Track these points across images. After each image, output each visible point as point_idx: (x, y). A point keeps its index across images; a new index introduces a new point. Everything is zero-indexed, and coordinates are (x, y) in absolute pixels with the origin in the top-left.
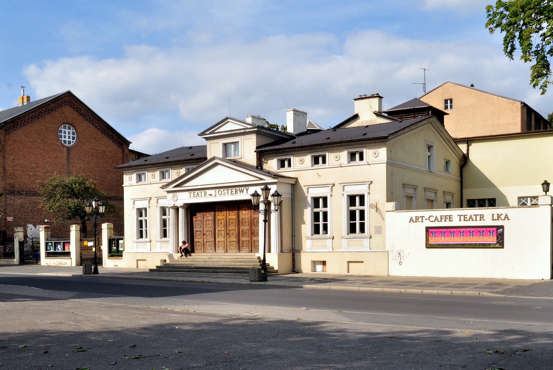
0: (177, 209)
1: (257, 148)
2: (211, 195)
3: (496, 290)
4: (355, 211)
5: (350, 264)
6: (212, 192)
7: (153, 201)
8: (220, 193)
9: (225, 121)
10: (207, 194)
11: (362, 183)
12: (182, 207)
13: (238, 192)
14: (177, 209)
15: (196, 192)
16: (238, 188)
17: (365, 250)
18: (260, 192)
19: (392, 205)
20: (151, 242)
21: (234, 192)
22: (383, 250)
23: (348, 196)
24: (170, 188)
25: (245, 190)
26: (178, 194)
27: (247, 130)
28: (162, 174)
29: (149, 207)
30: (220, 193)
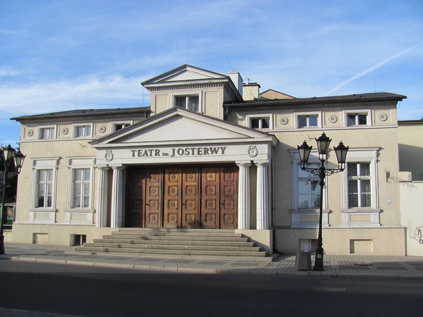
0: (109, 171)
1: (225, 103)
2: (166, 154)
4: (356, 181)
5: (404, 229)
6: (169, 151)
7: (64, 162)
8: (181, 152)
9: (182, 69)
10: (161, 153)
11: (369, 149)
12: (118, 168)
13: (209, 152)
14: (109, 171)
15: (144, 150)
16: (208, 147)
17: (374, 226)
19: (406, 175)
21: (203, 152)
23: (71, 235)
24: (104, 144)
25: (220, 151)
26: (114, 151)
27: (214, 81)
28: (77, 129)
29: (57, 169)
30: (181, 152)
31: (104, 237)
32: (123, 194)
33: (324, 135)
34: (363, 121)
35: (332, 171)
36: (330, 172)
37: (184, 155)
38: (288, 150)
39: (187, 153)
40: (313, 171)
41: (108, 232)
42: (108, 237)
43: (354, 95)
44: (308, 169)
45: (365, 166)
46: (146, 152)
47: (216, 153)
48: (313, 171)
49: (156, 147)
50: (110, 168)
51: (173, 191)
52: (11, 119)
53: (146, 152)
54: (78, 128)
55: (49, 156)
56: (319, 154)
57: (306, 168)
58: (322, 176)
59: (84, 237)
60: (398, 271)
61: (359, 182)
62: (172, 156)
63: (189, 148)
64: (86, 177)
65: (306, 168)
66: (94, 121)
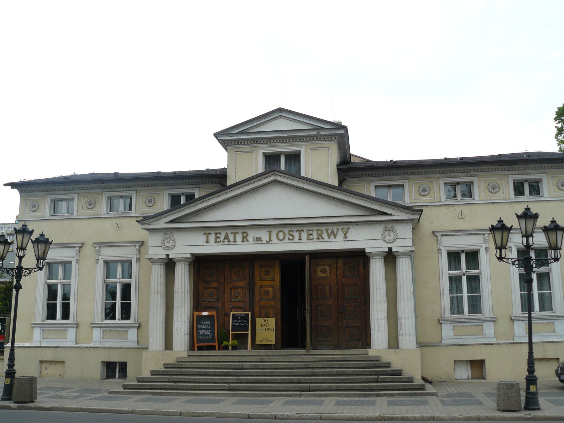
0: (170, 265)
2: (259, 239)
3: (48, 395)
6: (264, 235)
7: (88, 250)
10: (250, 238)
13: (325, 235)
14: (170, 265)
16: (323, 229)
18: (511, 221)
20: (77, 326)
22: (512, 341)
24: (162, 223)
31: (167, 366)
32: (190, 297)
33: (528, 209)
34: (468, 194)
35: (29, 271)
36: (28, 271)
37: (286, 240)
38: (433, 232)
39: (291, 238)
40: (9, 271)
41: (171, 358)
42: (173, 366)
43: (500, 155)
44: (508, 259)
45: (66, 265)
46: (226, 237)
47: (335, 237)
48: (9, 271)
49: (243, 229)
50: (171, 259)
51: (267, 293)
52: (5, 185)
53: (226, 237)
54: (55, 202)
55: (65, 241)
56: (523, 237)
57: (504, 258)
58: (19, 278)
59: (123, 366)
60: (472, 407)
61: (464, 279)
62: (268, 242)
63: (295, 229)
64: (67, 274)
65: (504, 258)
66: (200, 186)
